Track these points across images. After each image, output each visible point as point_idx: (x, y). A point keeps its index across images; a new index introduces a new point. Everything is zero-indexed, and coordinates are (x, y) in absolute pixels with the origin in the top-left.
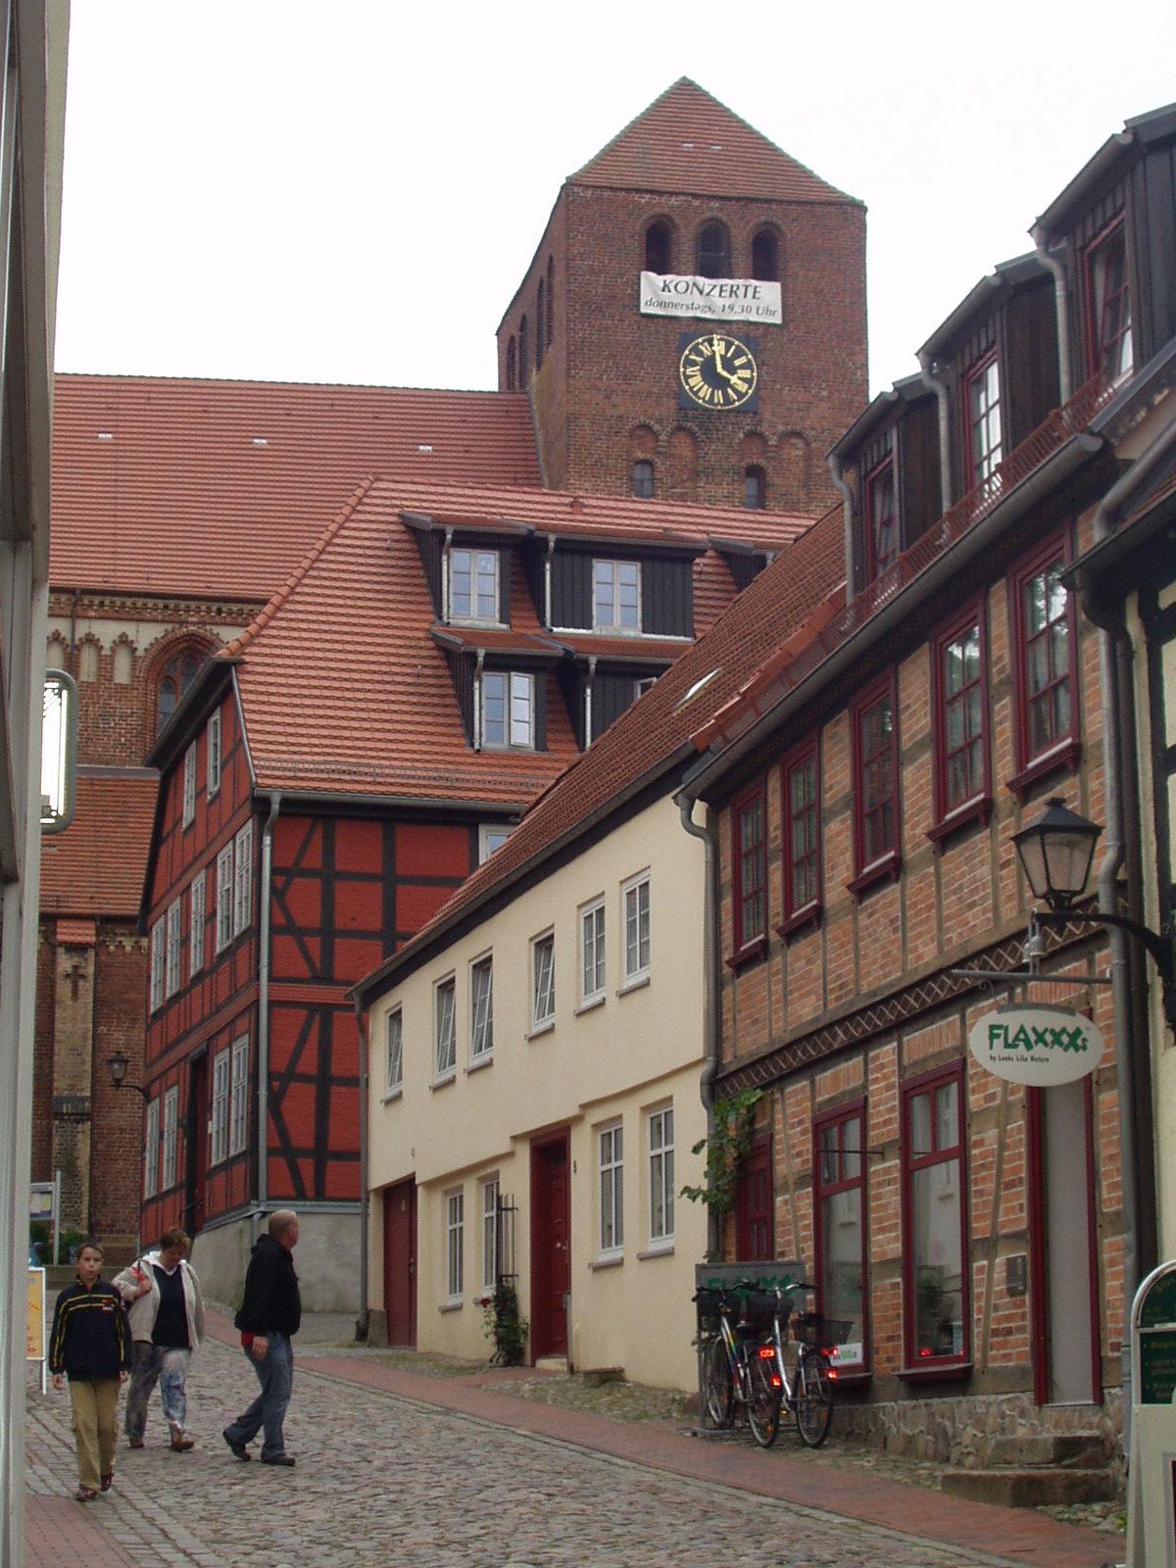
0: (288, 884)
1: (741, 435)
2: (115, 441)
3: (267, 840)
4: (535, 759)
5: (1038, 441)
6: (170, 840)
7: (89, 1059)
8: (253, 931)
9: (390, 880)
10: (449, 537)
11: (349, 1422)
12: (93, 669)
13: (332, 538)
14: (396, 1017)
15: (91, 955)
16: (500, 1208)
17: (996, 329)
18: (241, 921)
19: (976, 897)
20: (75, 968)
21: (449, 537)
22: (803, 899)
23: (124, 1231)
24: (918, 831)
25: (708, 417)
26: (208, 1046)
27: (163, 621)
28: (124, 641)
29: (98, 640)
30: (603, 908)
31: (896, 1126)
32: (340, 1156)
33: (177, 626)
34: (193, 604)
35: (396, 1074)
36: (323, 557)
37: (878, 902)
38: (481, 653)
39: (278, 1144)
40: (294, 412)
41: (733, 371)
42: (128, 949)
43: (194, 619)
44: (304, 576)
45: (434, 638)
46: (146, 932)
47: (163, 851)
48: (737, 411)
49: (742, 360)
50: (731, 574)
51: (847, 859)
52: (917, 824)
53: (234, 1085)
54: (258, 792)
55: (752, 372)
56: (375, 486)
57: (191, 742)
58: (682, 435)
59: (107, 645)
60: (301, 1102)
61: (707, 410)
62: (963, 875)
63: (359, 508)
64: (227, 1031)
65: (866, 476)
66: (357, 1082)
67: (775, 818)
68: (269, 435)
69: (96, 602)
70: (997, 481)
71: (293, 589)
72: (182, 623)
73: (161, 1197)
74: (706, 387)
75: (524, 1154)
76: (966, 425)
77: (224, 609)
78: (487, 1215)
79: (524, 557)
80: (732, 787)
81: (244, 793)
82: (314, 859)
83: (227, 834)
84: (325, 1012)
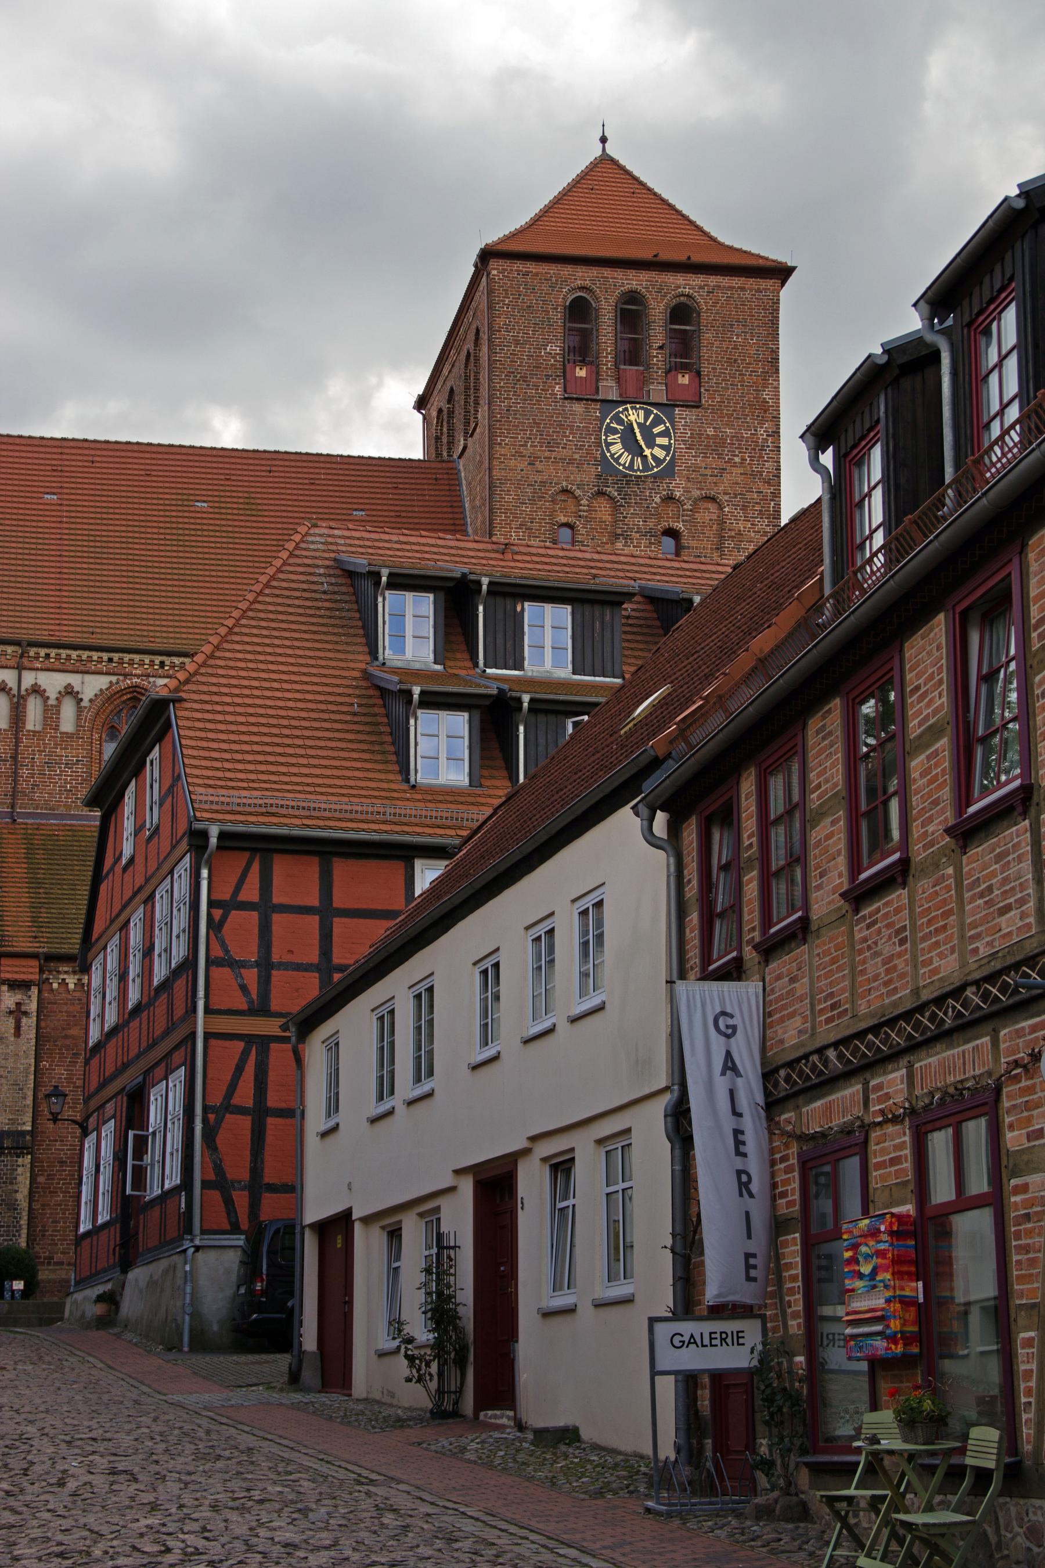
0: (224, 918)
1: (658, 500)
2: (59, 502)
3: (205, 873)
4: (469, 795)
5: (926, 515)
6: (110, 876)
7: (30, 1093)
8: (189, 964)
9: (326, 912)
10: (384, 579)
11: (277, 1506)
12: (39, 717)
13: (269, 581)
14: (333, 1047)
15: (35, 990)
16: (440, 1247)
17: (1019, 258)
18: (179, 952)
19: (1012, 900)
20: (18, 1004)
21: (384, 579)
22: (784, 911)
23: (62, 1263)
24: (931, 828)
25: (626, 480)
26: (144, 1079)
27: (107, 674)
28: (68, 691)
29: (45, 691)
30: (602, 900)
31: (907, 1165)
32: (272, 1188)
33: (121, 678)
34: (137, 658)
35: (333, 1105)
36: (260, 599)
37: (878, 910)
38: (416, 690)
39: (212, 1176)
40: (233, 478)
41: (651, 445)
42: (71, 986)
43: (138, 672)
44: (242, 617)
45: (366, 675)
46: (86, 969)
47: (103, 887)
48: (655, 476)
49: (661, 428)
50: (658, 618)
51: (841, 863)
52: (930, 820)
53: (169, 1117)
54: (198, 826)
55: (670, 439)
56: (311, 531)
57: (130, 781)
58: (601, 499)
59: (52, 694)
60: (237, 1129)
61: (626, 476)
62: (993, 875)
63: (297, 552)
64: (163, 1064)
65: (846, 455)
66: (293, 1113)
67: (749, 824)
68: (211, 499)
69: (42, 654)
70: (880, 560)
71: (231, 629)
72: (126, 675)
73: (96, 1230)
74: (626, 454)
75: (467, 1188)
76: (971, 381)
77: (167, 663)
78: (427, 1253)
79: (456, 599)
80: (695, 800)
81: (182, 827)
82: (251, 892)
83: (166, 868)
84: (263, 1042)
